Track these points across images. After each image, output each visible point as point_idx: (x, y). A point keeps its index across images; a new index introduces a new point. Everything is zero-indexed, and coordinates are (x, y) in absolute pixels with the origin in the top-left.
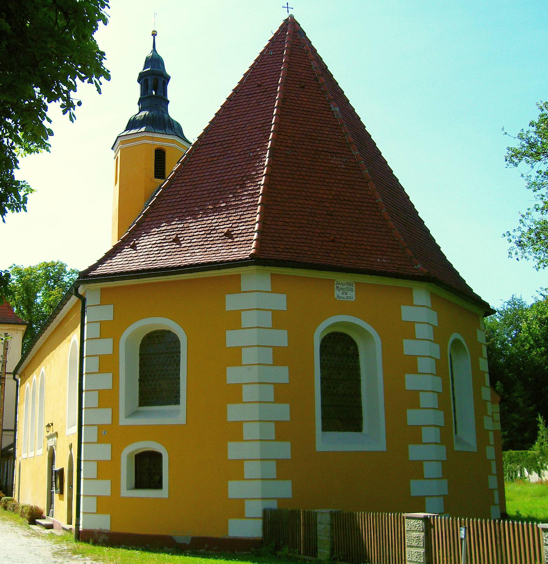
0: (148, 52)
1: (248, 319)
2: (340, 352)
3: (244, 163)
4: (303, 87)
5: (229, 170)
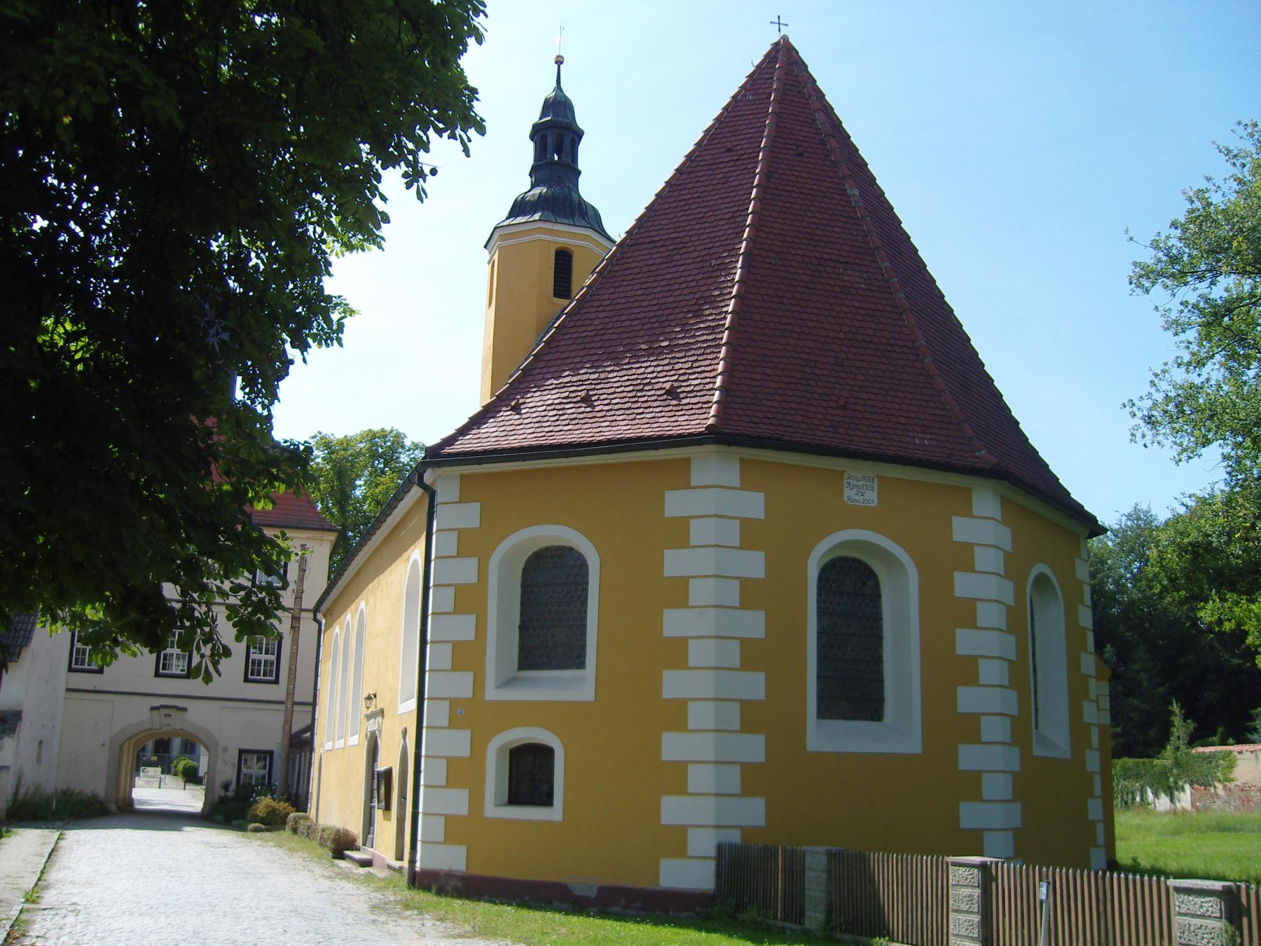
0: (548, 91)
1: (700, 532)
2: (850, 590)
3: (701, 276)
4: (801, 155)
5: (676, 286)
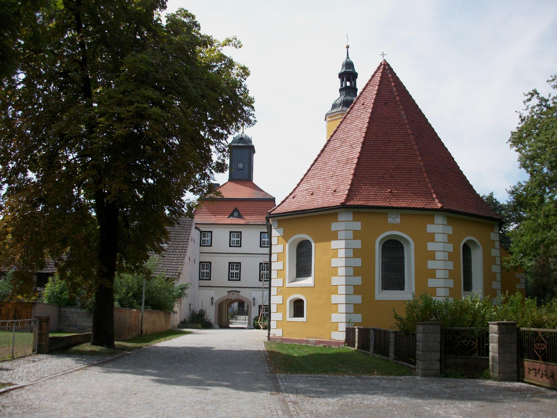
0: (343, 59)
2: (393, 249)
4: (386, 104)
